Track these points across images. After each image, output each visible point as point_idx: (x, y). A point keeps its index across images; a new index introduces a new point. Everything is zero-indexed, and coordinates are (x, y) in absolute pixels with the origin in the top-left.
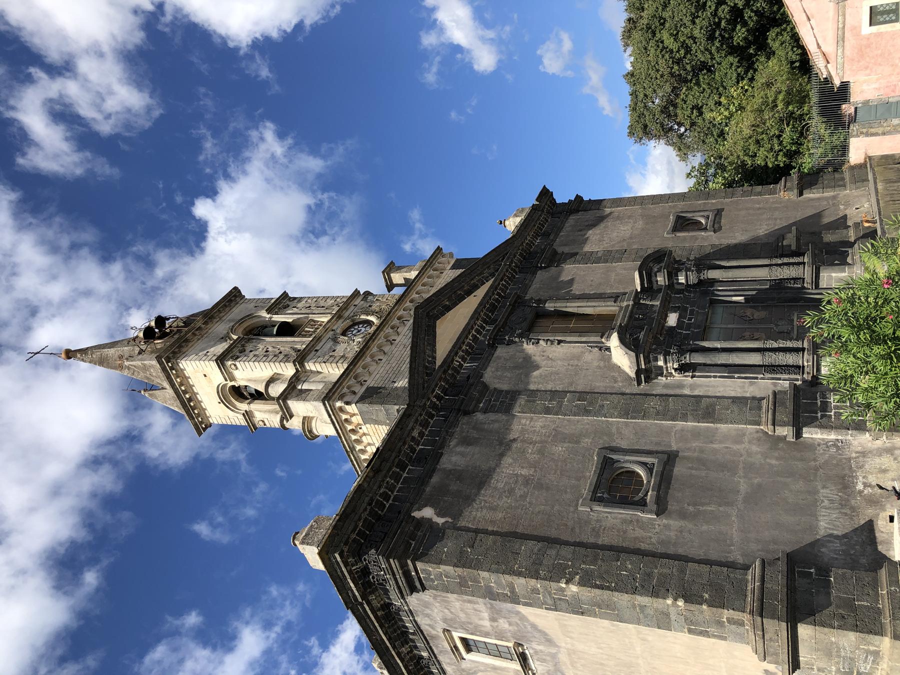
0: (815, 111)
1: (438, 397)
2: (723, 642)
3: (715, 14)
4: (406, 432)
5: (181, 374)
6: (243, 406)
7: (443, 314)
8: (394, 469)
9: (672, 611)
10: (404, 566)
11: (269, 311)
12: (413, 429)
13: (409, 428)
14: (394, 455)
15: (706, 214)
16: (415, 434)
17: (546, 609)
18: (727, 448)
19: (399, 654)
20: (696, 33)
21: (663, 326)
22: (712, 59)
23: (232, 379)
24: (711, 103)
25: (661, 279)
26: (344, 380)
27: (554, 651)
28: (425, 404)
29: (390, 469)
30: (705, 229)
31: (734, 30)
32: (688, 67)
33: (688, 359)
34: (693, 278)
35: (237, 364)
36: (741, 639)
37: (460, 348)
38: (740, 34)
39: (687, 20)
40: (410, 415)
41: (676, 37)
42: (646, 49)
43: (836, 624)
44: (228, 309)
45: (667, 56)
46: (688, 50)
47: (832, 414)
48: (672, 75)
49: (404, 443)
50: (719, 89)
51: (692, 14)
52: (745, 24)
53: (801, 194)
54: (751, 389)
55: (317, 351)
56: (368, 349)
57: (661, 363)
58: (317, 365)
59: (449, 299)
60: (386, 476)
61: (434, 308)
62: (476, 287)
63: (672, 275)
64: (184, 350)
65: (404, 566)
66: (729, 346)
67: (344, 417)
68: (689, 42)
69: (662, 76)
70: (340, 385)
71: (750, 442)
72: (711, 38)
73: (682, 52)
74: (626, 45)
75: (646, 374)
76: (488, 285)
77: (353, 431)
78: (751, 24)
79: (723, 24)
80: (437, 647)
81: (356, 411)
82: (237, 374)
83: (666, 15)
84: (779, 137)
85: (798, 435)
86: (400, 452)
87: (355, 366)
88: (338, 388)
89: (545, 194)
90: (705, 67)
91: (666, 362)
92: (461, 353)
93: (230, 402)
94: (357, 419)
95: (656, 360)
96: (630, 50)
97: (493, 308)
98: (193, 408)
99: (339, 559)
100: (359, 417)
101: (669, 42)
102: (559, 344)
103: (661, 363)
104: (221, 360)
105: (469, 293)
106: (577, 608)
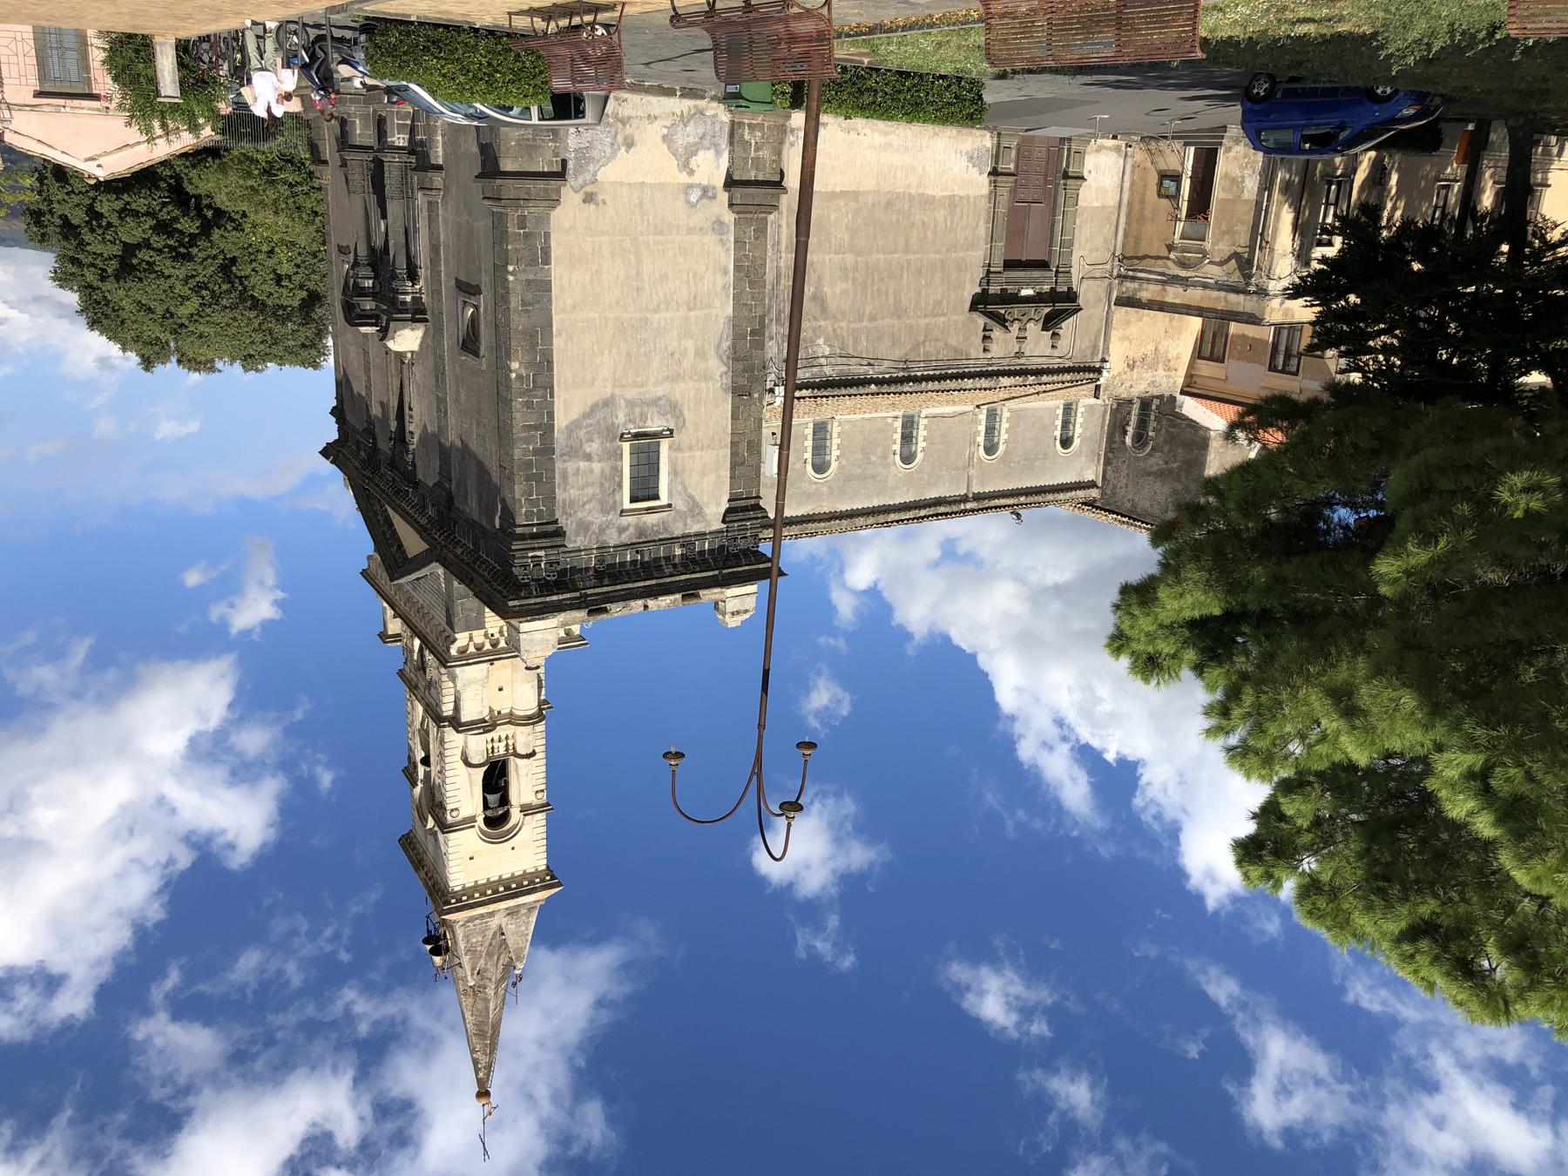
0: (264, 146)
2: (552, 236)
3: (160, 251)
5: (468, 892)
6: (515, 815)
9: (523, 277)
10: (523, 537)
11: (414, 784)
15: (460, 304)
17: (552, 396)
19: (671, 575)
20: (181, 272)
22: (215, 257)
23: (472, 819)
24: (270, 263)
25: (368, 305)
27: (623, 404)
30: (476, 307)
31: (181, 232)
32: (225, 287)
33: (402, 269)
34: (368, 272)
35: (449, 807)
36: (544, 220)
38: (188, 225)
39: (165, 285)
41: (185, 298)
42: (201, 337)
43: (941, 214)
45: (208, 310)
46: (201, 287)
48: (233, 307)
50: (252, 252)
51: (158, 277)
52: (176, 220)
53: (325, 162)
57: (409, 298)
58: (445, 700)
59: (391, 546)
62: (387, 518)
63: (362, 292)
65: (523, 537)
67: (472, 649)
68: (192, 283)
69: (234, 319)
72: (188, 257)
73: (204, 293)
74: (212, 369)
75: (417, 314)
76: (390, 511)
77: (494, 645)
78: (177, 212)
79: (171, 242)
80: (658, 532)
81: (466, 634)
82: (465, 812)
83: (160, 310)
84: (291, 186)
85: (439, 168)
89: (326, 452)
90: (227, 267)
91: (407, 294)
93: (510, 831)
94: (478, 636)
95: (404, 303)
96: (219, 365)
98: (520, 885)
99: (516, 603)
100: (475, 633)
101: (192, 305)
103: (409, 298)
104: (445, 827)
105: (391, 525)
106: (543, 366)
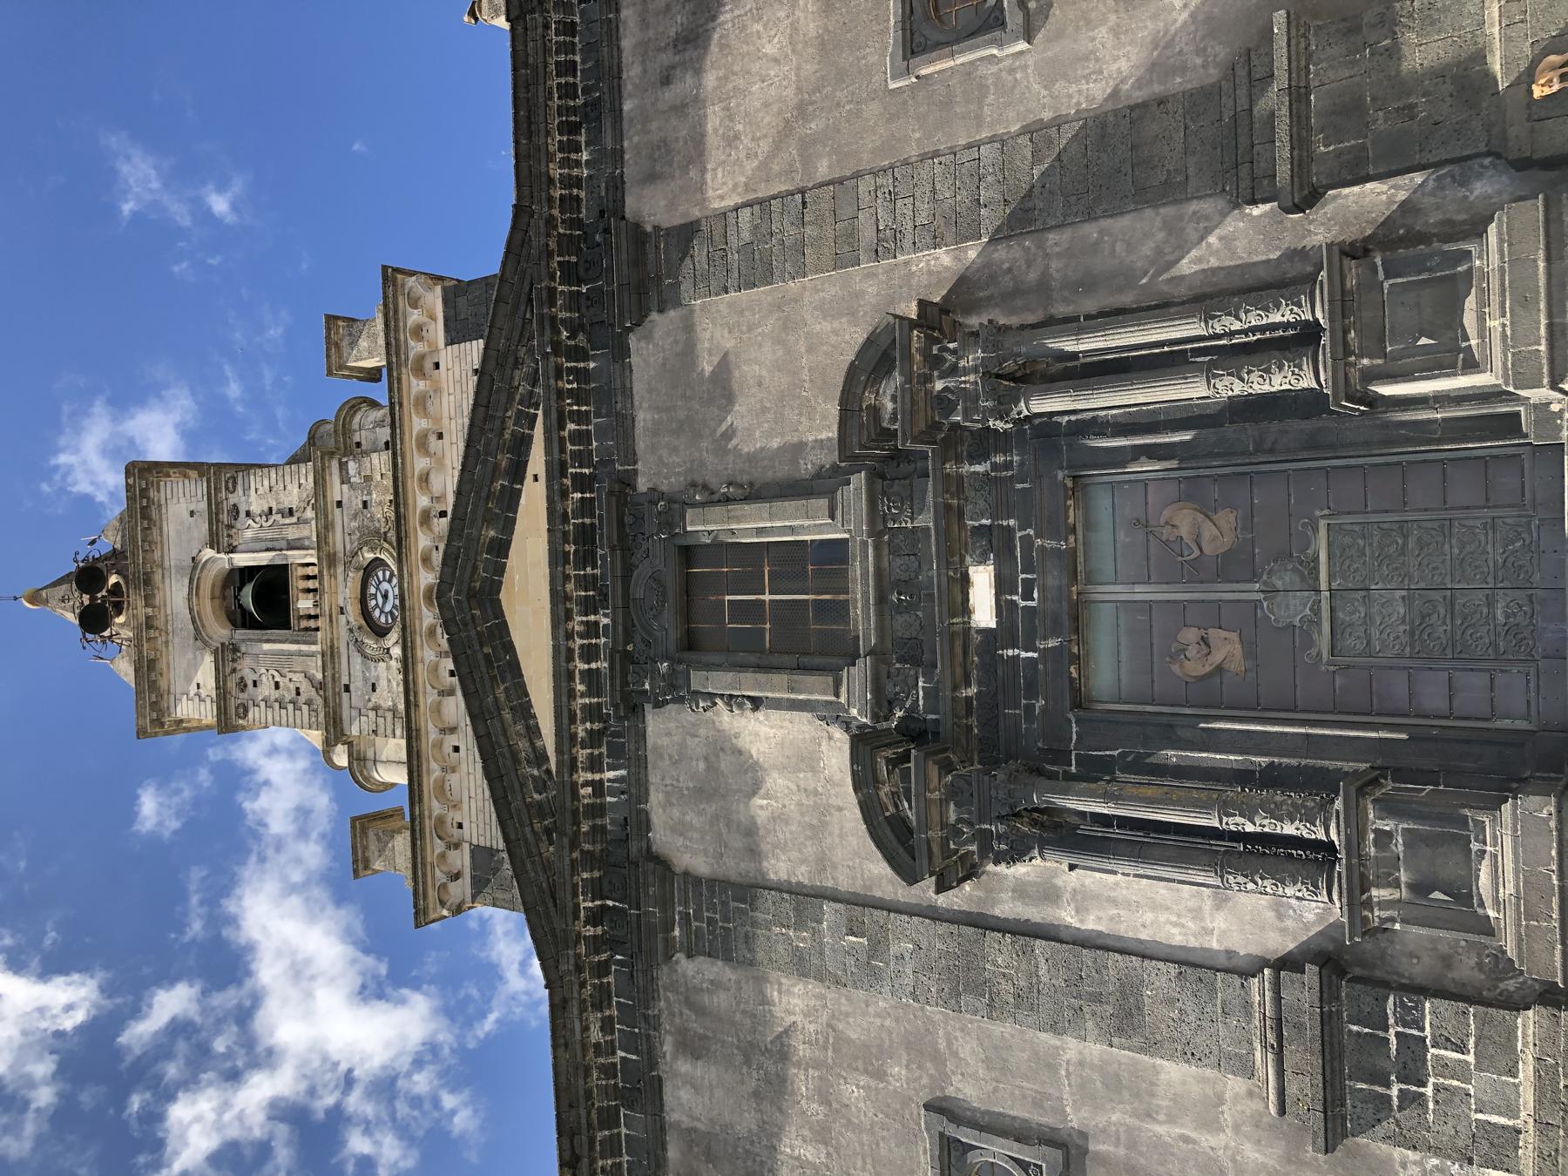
1: (595, 917)
4: (578, 1047)
7: (500, 570)
8: (600, 1135)
12: (586, 1029)
13: (578, 1037)
14: (583, 1112)
16: (596, 1035)
18: (1186, 1139)
21: (967, 630)
26: (423, 849)
28: (578, 956)
29: (592, 1141)
37: (573, 737)
40: (565, 1001)
44: (155, 531)
47: (1429, 1091)
49: (587, 1070)
54: (1220, 922)
55: (347, 688)
56: (418, 737)
59: (489, 520)
60: (592, 1162)
61: (475, 568)
64: (163, 684)
66: (1185, 334)
70: (424, 864)
71: (1237, 1128)
86: (588, 1094)
87: (421, 800)
88: (425, 875)
92: (582, 754)
97: (586, 536)
102: (756, 708)
